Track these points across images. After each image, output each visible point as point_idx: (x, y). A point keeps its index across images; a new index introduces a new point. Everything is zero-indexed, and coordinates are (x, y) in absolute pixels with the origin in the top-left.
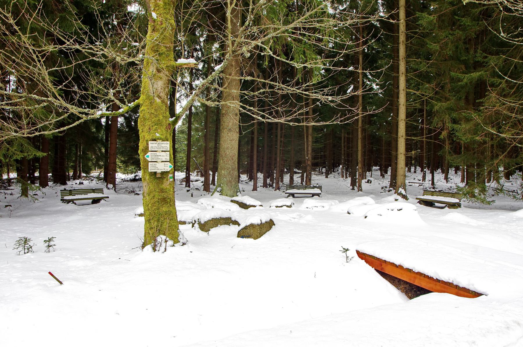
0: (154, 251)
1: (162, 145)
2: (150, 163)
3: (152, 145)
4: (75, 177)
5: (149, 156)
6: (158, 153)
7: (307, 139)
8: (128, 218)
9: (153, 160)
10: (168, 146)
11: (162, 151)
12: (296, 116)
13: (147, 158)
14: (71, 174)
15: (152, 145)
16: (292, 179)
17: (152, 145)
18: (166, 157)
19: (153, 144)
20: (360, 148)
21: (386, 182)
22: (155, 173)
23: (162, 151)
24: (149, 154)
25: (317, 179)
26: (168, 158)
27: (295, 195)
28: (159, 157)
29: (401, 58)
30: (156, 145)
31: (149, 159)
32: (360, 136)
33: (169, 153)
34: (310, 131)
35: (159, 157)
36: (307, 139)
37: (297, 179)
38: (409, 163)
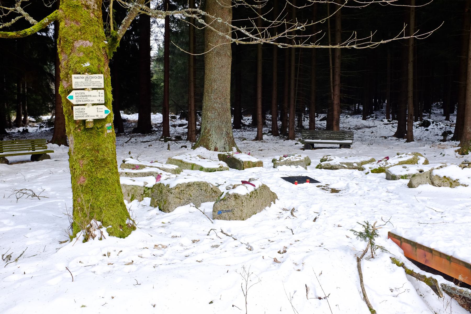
0: (389, 233)
1: (93, 80)
2: (74, 107)
3: (77, 80)
4: (17, 124)
5: (74, 97)
6: (86, 92)
7: (333, 64)
8: (51, 181)
9: (79, 103)
10: (102, 81)
11: (93, 89)
12: (284, 34)
13: (71, 101)
14: (14, 118)
15: (77, 80)
16: (312, 122)
17: (77, 80)
18: (99, 98)
19: (78, 78)
20: (411, 76)
21: (392, 129)
22: (84, 122)
23: (93, 89)
24: (73, 93)
25: (348, 121)
26: (102, 100)
27: (316, 145)
28: (89, 98)
29: (49, 16)
30: (83, 80)
31: (74, 102)
32: (411, 59)
33: (103, 91)
34: (338, 54)
35: (89, 98)
36: (333, 64)
37: (321, 123)
38: (342, 107)
